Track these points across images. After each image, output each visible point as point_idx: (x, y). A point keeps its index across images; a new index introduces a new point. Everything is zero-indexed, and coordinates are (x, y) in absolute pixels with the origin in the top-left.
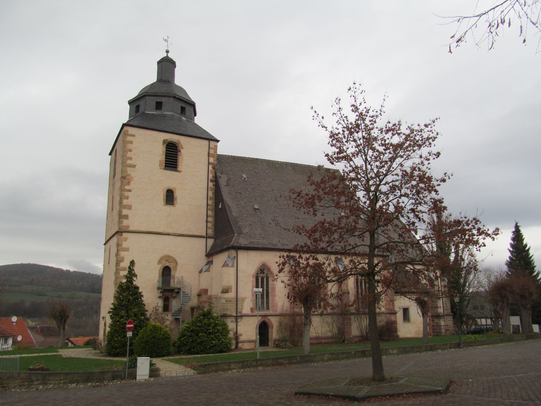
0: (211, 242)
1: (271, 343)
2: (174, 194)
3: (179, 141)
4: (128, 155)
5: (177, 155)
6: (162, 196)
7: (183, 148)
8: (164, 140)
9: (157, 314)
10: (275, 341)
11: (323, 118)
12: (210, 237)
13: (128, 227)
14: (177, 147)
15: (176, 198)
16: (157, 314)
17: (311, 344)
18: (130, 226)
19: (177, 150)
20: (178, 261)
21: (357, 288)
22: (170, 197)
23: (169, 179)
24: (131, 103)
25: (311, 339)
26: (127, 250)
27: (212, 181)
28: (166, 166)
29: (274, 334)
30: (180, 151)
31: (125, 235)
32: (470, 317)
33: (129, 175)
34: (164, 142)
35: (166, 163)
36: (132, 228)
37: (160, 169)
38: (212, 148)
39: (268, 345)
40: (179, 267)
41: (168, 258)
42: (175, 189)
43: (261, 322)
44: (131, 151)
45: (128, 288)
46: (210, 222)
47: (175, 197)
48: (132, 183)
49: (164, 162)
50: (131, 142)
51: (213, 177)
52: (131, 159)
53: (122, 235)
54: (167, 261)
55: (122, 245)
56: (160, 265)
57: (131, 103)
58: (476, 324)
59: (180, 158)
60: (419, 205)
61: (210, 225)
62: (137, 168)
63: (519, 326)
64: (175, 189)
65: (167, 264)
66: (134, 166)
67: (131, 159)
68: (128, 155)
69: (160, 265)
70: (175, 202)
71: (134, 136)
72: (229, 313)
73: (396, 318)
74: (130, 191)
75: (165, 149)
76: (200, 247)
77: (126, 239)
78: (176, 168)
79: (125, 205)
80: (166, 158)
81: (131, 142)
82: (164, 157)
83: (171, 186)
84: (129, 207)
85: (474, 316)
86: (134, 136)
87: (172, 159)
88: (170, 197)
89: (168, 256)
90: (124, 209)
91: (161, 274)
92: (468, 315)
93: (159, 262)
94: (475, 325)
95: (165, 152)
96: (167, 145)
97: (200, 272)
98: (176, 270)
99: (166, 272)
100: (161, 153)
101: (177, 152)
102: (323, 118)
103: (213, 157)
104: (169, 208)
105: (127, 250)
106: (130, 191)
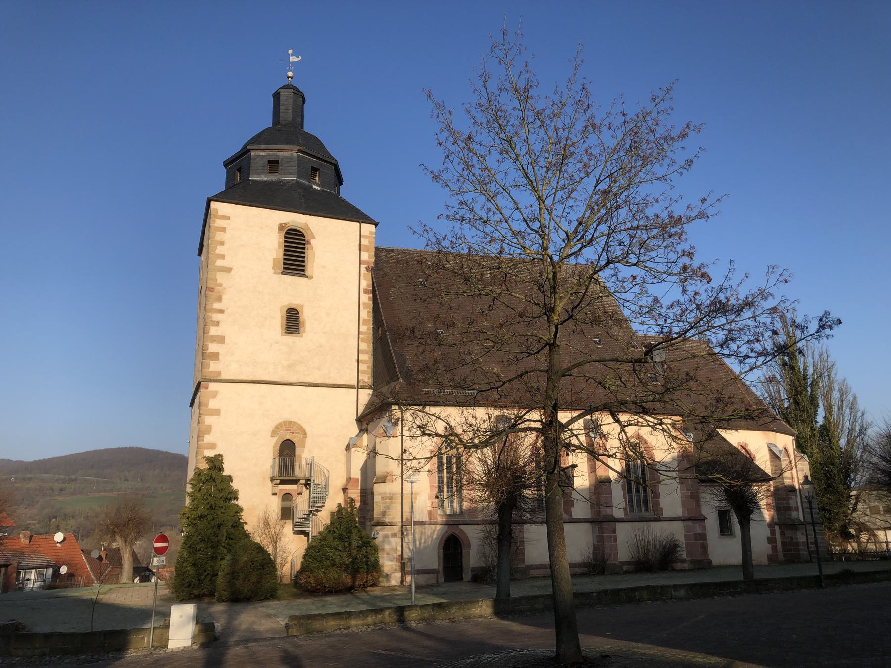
0: (365, 396)
1: (467, 576)
2: (301, 315)
3: (307, 225)
4: (218, 252)
5: (304, 249)
6: (278, 320)
7: (314, 237)
8: (281, 224)
9: (267, 524)
10: (473, 569)
11: (450, 113)
12: (363, 388)
13: (219, 373)
14: (303, 235)
15: (304, 322)
16: (267, 524)
17: (574, 575)
18: (222, 372)
19: (304, 240)
20: (308, 430)
21: (630, 491)
22: (293, 321)
23: (292, 290)
24: (227, 164)
25: (572, 565)
26: (217, 412)
27: (366, 292)
28: (284, 268)
29: (474, 558)
30: (309, 243)
31: (213, 386)
32: (862, 527)
33: (220, 285)
34: (281, 227)
35: (285, 264)
36: (224, 376)
37: (277, 273)
38: (366, 237)
39: (461, 579)
40: (308, 441)
41: (289, 425)
42: (302, 306)
43: (447, 535)
44: (222, 244)
45: (211, 479)
46: (364, 362)
47: (301, 320)
48: (224, 298)
49: (282, 261)
50: (223, 229)
51: (368, 286)
52: (223, 257)
53: (207, 388)
54: (288, 430)
55: (207, 405)
56: (275, 439)
57: (227, 164)
58: (877, 542)
59: (309, 254)
60: (208, 439)
61: (363, 367)
62: (232, 272)
63: (357, 480)
64: (302, 306)
65: (288, 437)
66: (229, 270)
67: (223, 257)
68: (218, 252)
69: (275, 439)
70: (302, 329)
71: (228, 218)
72: (395, 520)
73: (704, 528)
74: (222, 311)
75: (282, 240)
76: (350, 404)
77: (215, 395)
78: (303, 270)
79: (212, 337)
80: (285, 255)
81: (223, 229)
82: (281, 252)
83: (295, 302)
84: (221, 340)
85: (872, 526)
86: (228, 218)
87: (295, 255)
88: (293, 321)
89: (290, 422)
90: (212, 342)
91: (277, 454)
92: (857, 524)
93: (274, 433)
94: (875, 543)
95: (283, 244)
96: (286, 233)
97: (348, 448)
98: (303, 445)
99: (287, 451)
100: (276, 246)
101: (304, 244)
102: (450, 113)
103: (367, 251)
104: (291, 339)
105: (217, 412)
106: (222, 311)
